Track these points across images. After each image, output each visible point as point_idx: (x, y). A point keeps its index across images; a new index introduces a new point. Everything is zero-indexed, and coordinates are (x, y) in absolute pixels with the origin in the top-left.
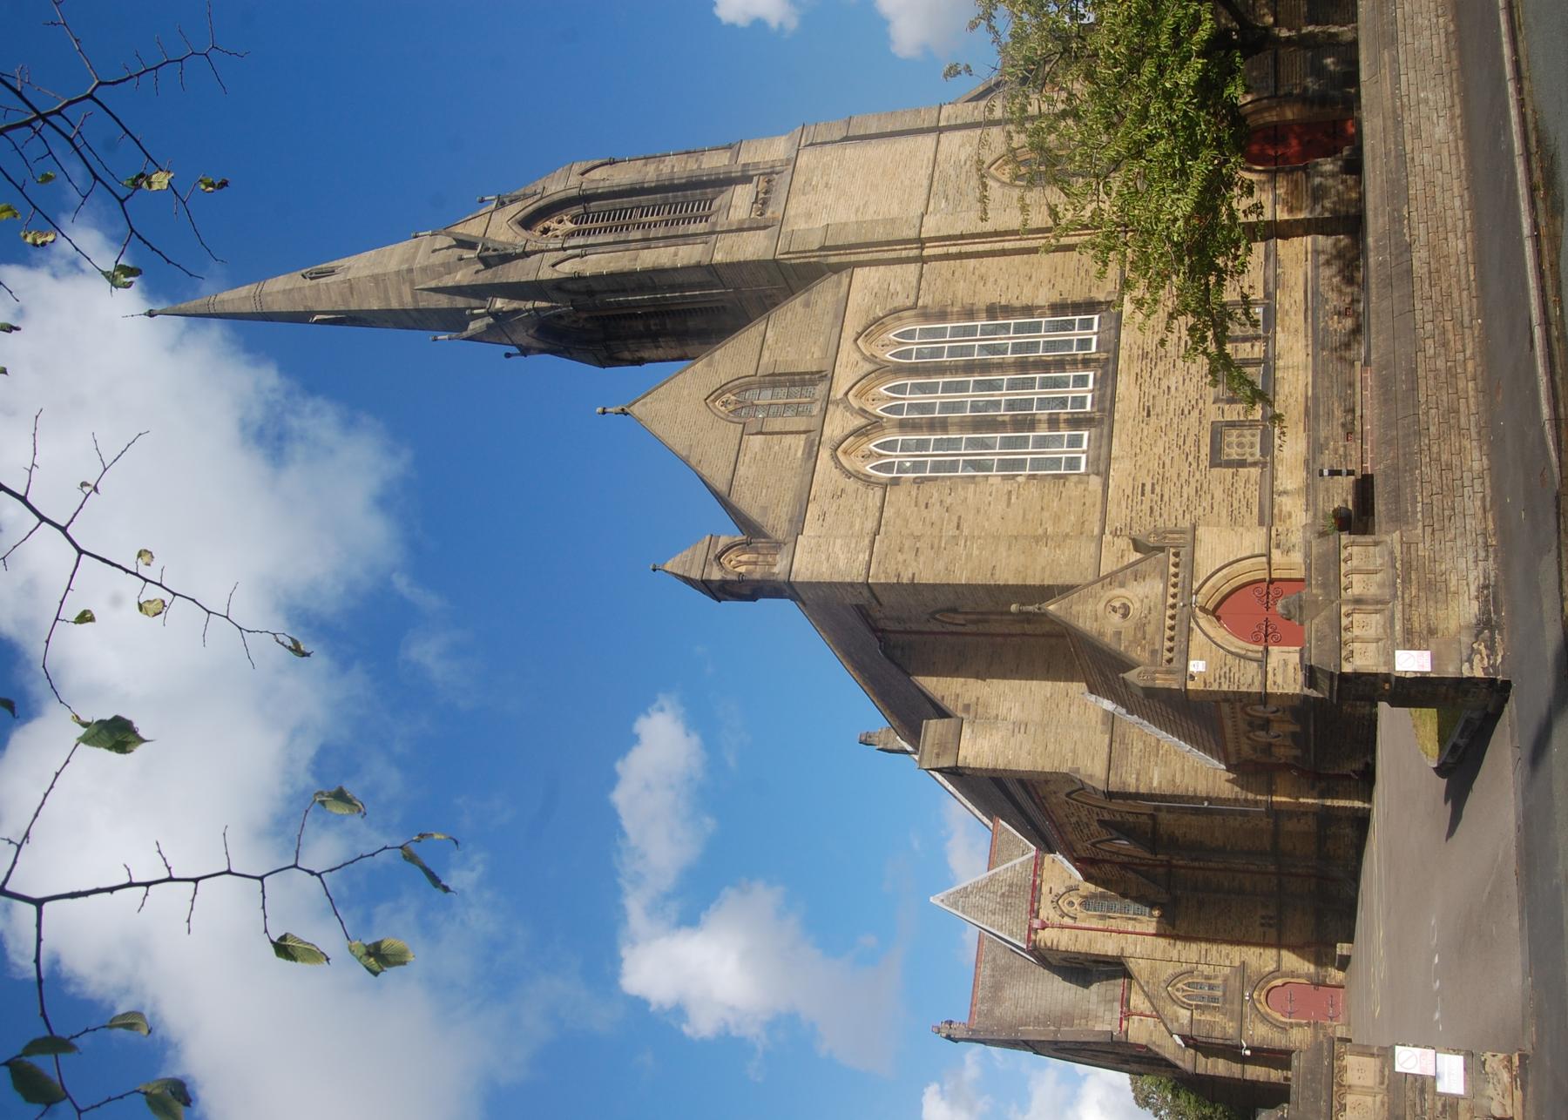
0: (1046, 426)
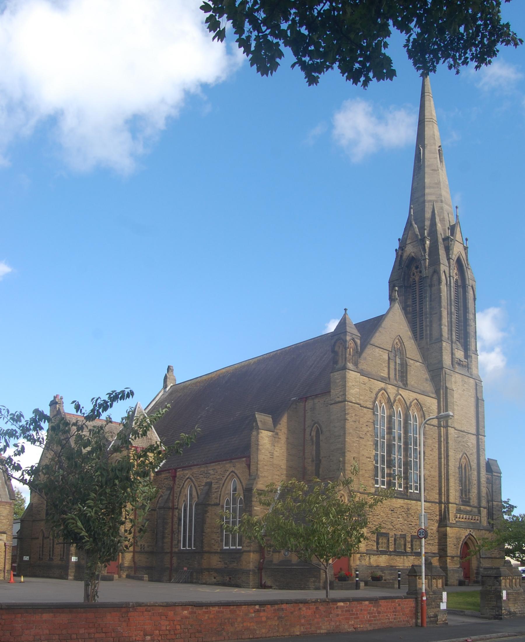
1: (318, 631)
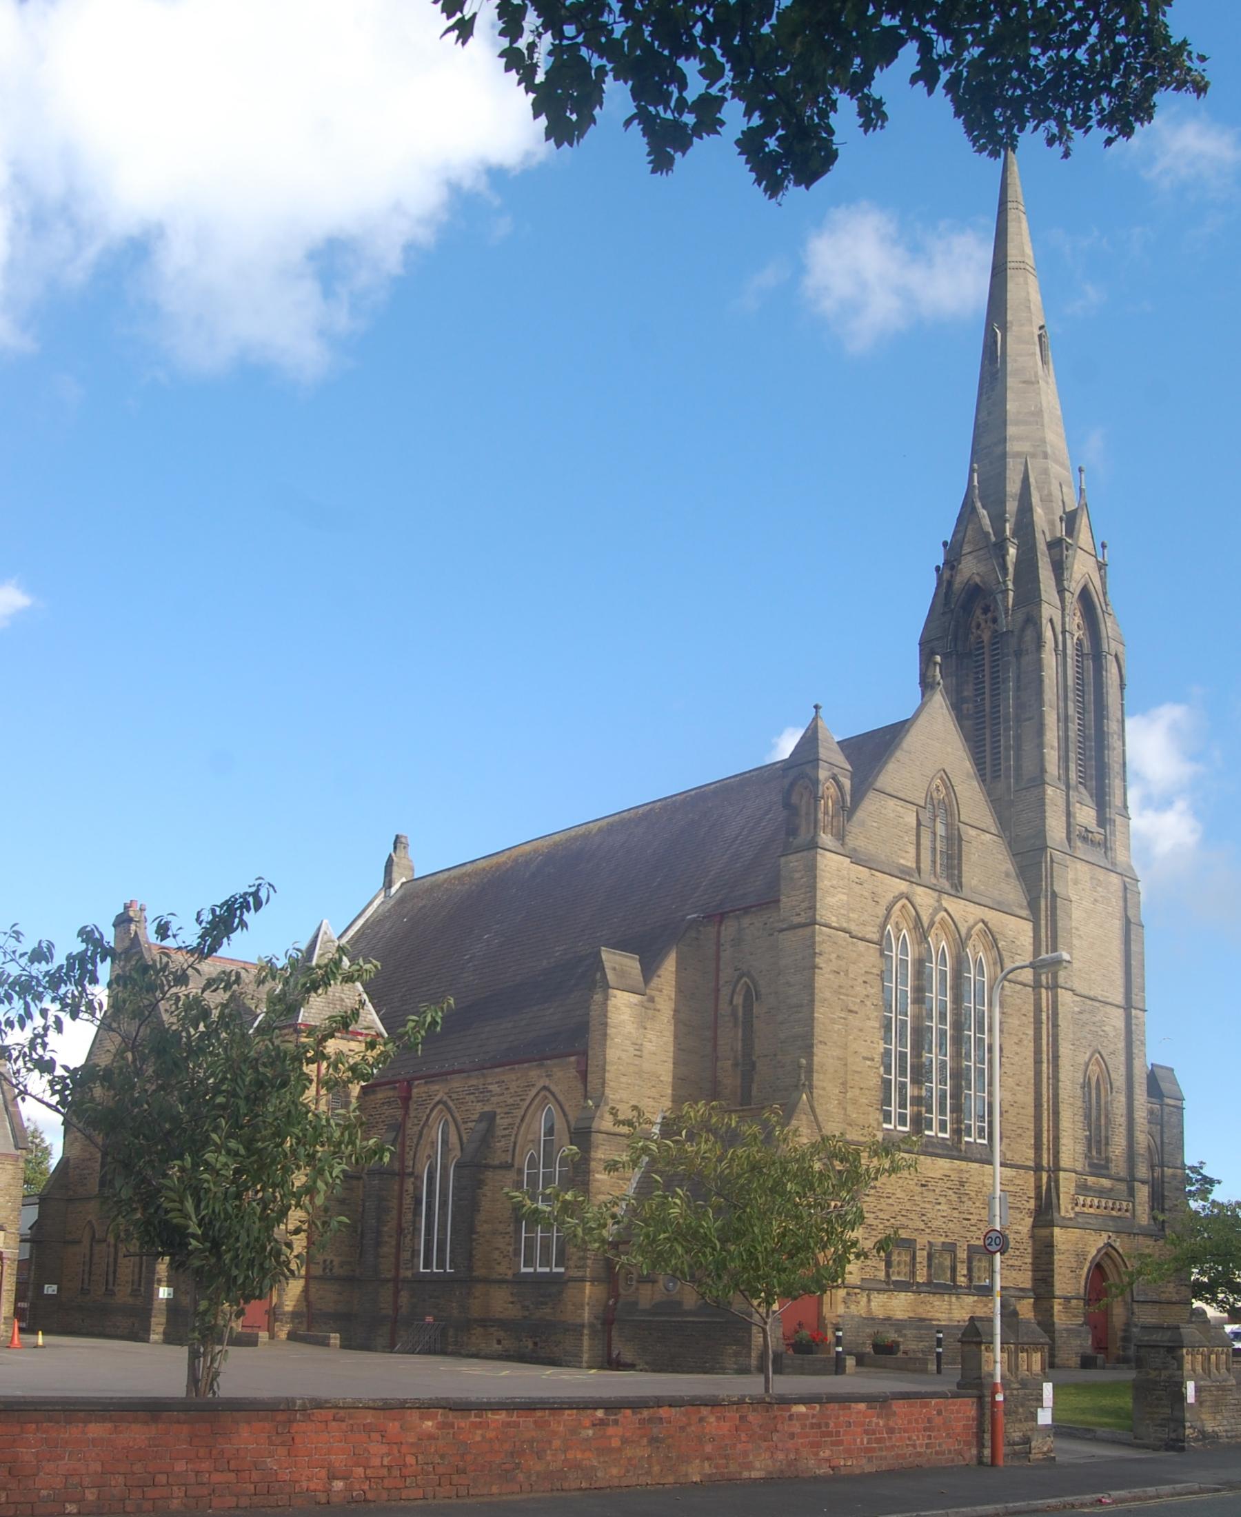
0: (916, 1094)
1: (746, 1474)
